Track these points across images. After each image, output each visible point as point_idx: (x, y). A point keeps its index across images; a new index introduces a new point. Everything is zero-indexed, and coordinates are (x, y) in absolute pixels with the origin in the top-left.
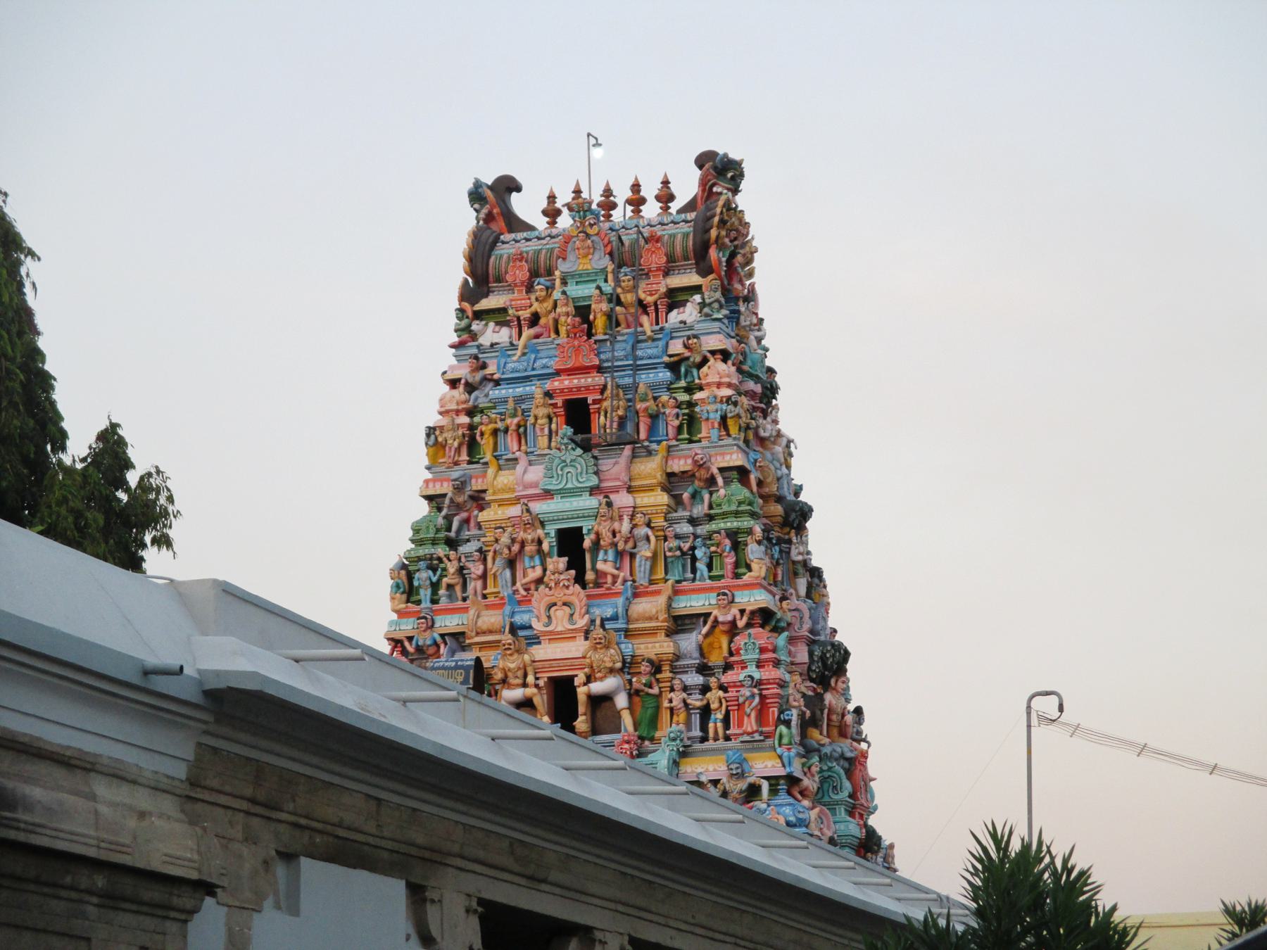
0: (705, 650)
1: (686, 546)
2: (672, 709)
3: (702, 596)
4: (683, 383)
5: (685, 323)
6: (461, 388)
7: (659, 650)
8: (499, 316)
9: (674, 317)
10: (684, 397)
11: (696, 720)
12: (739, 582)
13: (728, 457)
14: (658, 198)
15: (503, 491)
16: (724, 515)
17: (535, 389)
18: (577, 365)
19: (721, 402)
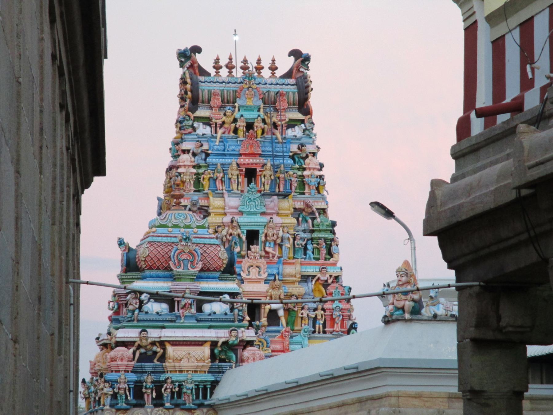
0: (37, 302)
1: (304, 243)
2: (302, 318)
3: (312, 267)
4: (297, 166)
5: (296, 136)
6: (190, 154)
7: (299, 291)
9: (290, 133)
10: (299, 173)
11: (311, 323)
12: (327, 262)
13: (320, 204)
14: (270, 68)
15: (217, 208)
16: (320, 231)
17: (234, 161)
18: (251, 152)
19: (317, 177)
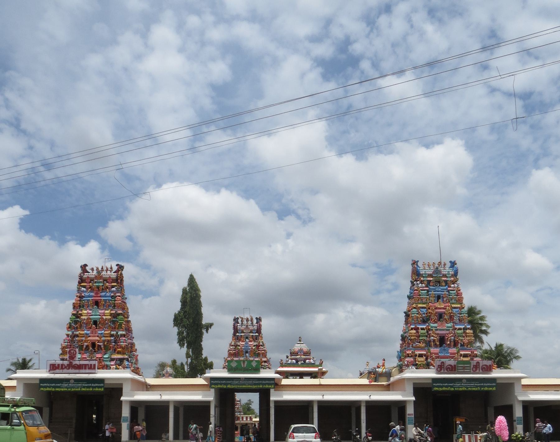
8: (84, 287)
